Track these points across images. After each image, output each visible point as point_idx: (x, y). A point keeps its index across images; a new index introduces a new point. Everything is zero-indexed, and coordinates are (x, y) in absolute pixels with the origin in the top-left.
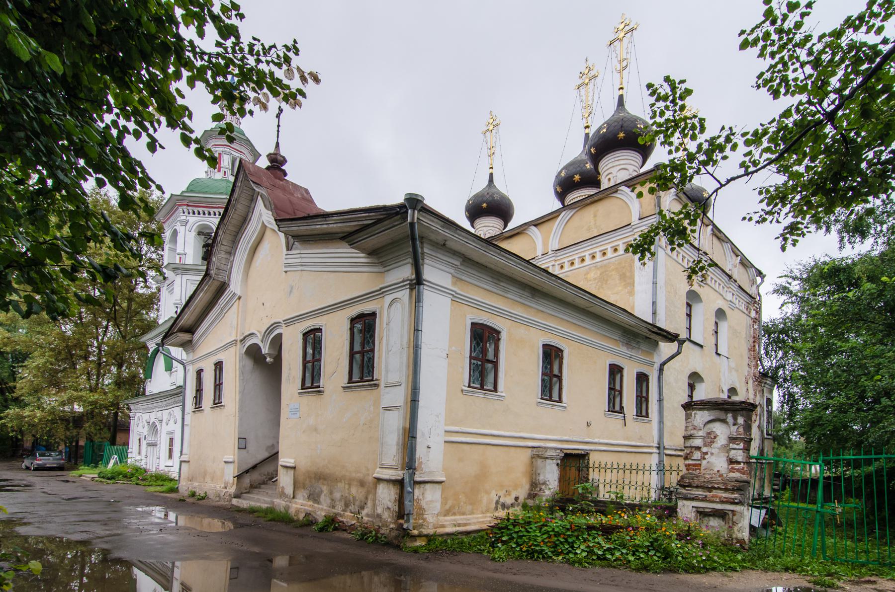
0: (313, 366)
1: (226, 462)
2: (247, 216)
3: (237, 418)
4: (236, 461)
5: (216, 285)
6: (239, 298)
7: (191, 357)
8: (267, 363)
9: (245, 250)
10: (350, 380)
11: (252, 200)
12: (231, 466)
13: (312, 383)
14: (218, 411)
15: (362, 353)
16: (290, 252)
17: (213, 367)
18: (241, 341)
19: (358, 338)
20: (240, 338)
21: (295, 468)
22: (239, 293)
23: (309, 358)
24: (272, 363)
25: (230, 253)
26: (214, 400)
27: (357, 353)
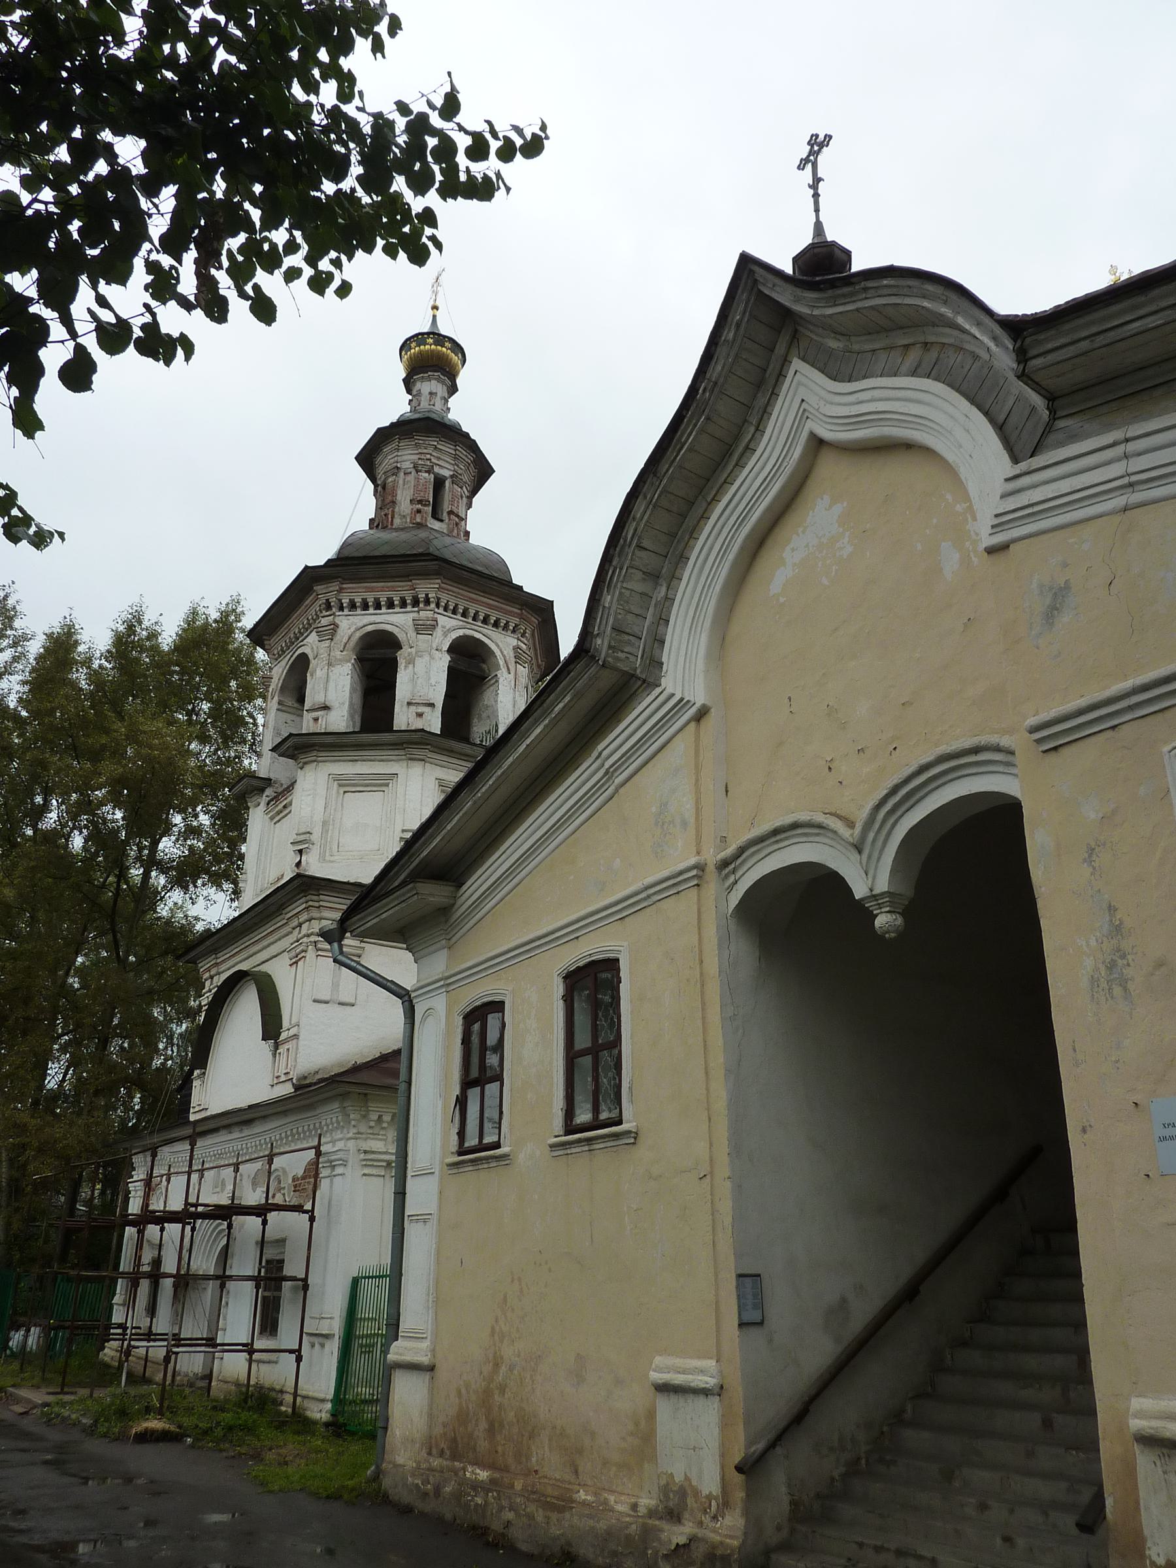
0: (190, 1166)
1: (665, 1388)
2: (737, 437)
3: (725, 1188)
4: (737, 1391)
5: (607, 680)
6: (701, 715)
7: (439, 963)
8: (878, 938)
9: (724, 550)
10: (570, 1129)
11: (759, 385)
12: (708, 1413)
13: (596, 1110)
14: (597, 1168)
15: (594, 1051)
16: (1023, 466)
17: (559, 989)
18: (724, 864)
19: (582, 1020)
20: (712, 856)
21: (431, 1368)
22: (699, 696)
23: (583, 1040)
24: (902, 936)
25: (654, 577)
26: (569, 1113)
27: (583, 1053)
